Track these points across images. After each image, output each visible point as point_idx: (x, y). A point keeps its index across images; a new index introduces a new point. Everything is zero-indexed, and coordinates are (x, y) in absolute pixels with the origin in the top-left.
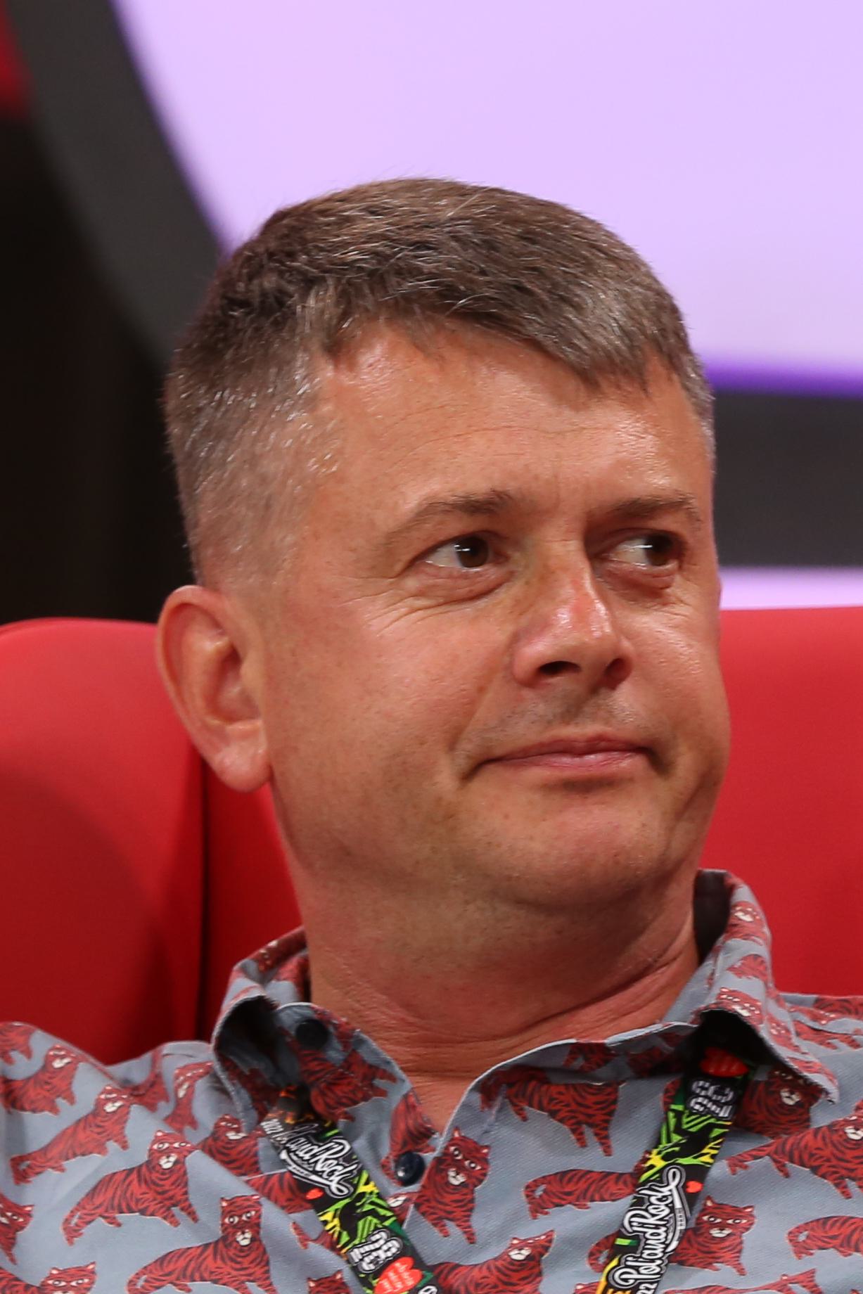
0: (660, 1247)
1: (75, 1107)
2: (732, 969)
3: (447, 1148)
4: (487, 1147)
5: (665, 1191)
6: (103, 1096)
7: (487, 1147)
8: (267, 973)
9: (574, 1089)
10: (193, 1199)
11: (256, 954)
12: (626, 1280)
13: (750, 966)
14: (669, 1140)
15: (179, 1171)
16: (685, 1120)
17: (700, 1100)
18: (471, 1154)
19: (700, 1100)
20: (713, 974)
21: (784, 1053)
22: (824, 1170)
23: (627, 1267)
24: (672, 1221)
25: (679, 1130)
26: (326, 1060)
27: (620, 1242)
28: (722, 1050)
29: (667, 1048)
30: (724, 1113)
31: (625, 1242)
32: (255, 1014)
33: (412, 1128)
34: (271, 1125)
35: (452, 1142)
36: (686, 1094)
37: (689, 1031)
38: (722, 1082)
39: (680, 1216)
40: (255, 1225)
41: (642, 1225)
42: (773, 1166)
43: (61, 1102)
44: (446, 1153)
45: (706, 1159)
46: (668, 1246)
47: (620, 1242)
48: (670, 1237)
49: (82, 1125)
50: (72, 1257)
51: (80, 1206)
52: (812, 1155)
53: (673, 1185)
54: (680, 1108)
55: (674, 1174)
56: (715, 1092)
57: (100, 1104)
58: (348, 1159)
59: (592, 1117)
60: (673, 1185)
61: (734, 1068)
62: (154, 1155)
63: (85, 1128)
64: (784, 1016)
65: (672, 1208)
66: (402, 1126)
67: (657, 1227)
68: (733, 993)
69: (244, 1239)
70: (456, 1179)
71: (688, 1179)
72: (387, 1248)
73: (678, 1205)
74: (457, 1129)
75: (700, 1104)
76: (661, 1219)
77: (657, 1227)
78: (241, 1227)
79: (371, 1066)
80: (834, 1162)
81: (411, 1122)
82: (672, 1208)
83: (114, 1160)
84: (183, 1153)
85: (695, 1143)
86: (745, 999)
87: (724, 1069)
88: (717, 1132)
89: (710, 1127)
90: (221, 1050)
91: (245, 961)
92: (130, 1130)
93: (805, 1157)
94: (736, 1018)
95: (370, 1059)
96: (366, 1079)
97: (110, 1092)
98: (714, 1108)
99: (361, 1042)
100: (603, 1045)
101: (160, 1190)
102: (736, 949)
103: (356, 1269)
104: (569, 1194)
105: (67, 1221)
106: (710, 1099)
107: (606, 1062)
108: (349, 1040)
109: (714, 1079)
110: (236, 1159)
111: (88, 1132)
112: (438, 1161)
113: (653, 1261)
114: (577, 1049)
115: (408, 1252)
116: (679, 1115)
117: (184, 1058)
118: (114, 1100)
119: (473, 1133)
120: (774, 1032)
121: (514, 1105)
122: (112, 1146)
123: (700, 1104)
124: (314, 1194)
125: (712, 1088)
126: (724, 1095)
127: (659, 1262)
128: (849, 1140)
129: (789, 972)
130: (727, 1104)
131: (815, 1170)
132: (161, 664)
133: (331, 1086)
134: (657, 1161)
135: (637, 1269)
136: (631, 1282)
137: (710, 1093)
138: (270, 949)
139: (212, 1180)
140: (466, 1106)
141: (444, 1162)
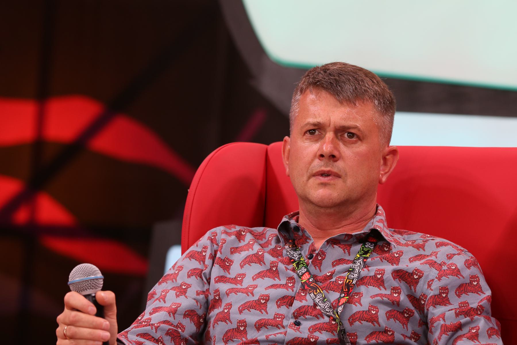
8: (291, 217)
9: (344, 241)
10: (265, 260)
13: (381, 221)
15: (262, 256)
18: (322, 253)
21: (386, 238)
25: (363, 250)
28: (375, 236)
29: (363, 236)
30: (372, 248)
32: (287, 223)
34: (287, 247)
35: (320, 251)
36: (365, 244)
38: (372, 243)
40: (277, 266)
43: (242, 241)
44: (319, 253)
50: (242, 271)
51: (243, 261)
57: (249, 242)
58: (300, 254)
62: (258, 252)
64: (388, 231)
65: (361, 264)
69: (274, 269)
70: (320, 258)
72: (304, 270)
78: (274, 267)
82: (361, 264)
83: (251, 252)
84: (264, 252)
85: (366, 253)
86: (379, 227)
89: (369, 250)
90: (279, 230)
94: (377, 230)
95: (307, 235)
96: (305, 239)
101: (258, 259)
102: (378, 218)
103: (298, 275)
105: (240, 264)
108: (303, 231)
110: (274, 253)
112: (317, 254)
114: (346, 235)
115: (308, 271)
116: (363, 248)
117: (271, 232)
119: (324, 250)
122: (250, 250)
124: (292, 260)
129: (391, 223)
132: (282, 151)
134: (358, 256)
139: (268, 258)
140: (324, 244)
141: (318, 255)
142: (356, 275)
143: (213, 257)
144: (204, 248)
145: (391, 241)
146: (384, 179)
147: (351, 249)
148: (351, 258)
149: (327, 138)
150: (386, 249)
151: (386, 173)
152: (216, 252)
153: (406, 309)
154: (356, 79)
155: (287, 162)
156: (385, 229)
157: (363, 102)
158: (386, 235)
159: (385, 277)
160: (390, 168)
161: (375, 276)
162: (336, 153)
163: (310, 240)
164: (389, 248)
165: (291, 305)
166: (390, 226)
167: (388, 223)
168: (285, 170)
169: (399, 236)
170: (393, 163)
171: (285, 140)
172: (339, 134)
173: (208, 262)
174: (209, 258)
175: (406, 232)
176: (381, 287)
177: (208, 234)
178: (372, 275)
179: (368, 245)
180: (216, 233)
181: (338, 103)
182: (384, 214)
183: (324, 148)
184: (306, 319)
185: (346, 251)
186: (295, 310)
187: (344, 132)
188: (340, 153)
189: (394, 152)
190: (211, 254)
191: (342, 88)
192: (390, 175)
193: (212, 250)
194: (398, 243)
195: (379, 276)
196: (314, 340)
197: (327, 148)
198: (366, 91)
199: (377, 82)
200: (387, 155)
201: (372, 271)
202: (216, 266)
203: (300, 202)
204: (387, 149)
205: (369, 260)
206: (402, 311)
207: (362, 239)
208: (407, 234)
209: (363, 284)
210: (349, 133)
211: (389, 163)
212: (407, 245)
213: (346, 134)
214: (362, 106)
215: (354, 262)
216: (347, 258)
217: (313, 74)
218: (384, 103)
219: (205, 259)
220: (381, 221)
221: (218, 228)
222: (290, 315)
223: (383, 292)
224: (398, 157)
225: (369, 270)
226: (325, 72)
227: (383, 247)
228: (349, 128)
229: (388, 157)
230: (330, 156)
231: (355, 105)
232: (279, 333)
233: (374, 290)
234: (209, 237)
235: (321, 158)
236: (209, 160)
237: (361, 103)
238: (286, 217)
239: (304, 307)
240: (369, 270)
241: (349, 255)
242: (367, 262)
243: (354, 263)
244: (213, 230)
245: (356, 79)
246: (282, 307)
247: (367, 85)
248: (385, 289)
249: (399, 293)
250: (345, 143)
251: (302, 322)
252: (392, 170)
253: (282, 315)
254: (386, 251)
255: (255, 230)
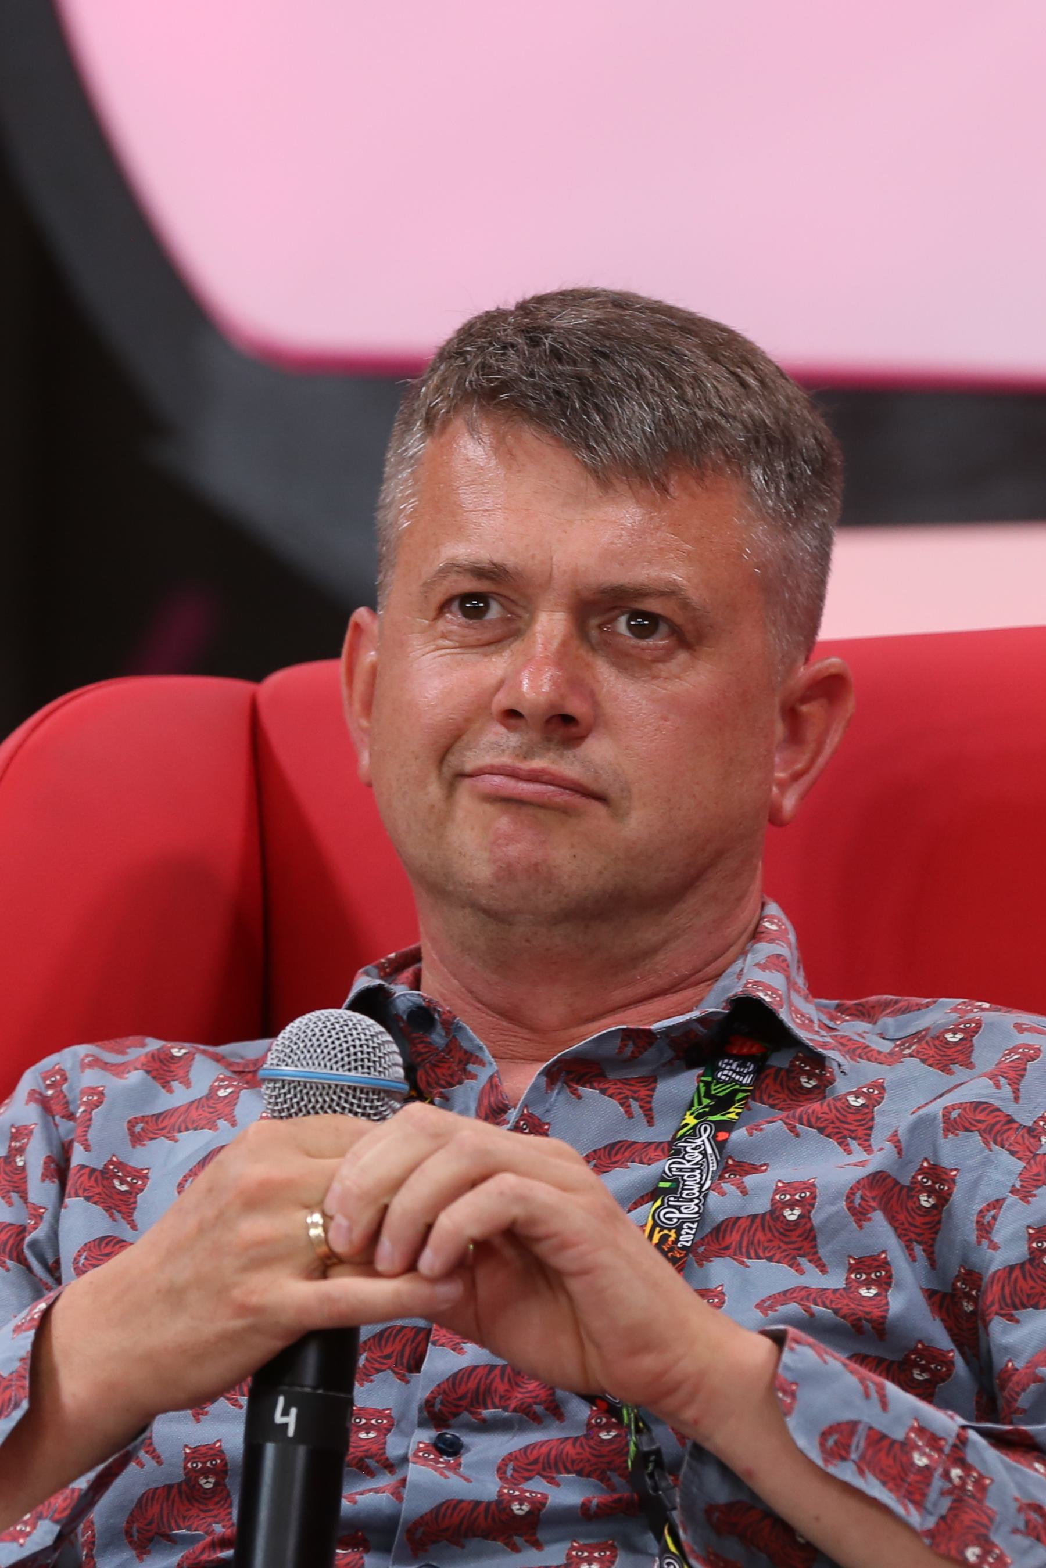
0: (697, 1187)
1: (190, 1090)
2: (757, 965)
3: (518, 1122)
4: (548, 1124)
5: (699, 1142)
6: (216, 1084)
7: (548, 1124)
11: (377, 962)
12: (670, 1219)
13: (776, 963)
14: (700, 1103)
16: (713, 1087)
17: (726, 1072)
19: (726, 1072)
20: (742, 970)
21: (803, 1035)
22: (829, 1130)
23: (669, 1206)
24: (705, 1164)
25: (708, 1095)
26: (430, 1043)
27: (662, 1185)
28: (751, 1027)
29: (701, 1030)
30: (747, 1080)
31: (667, 1185)
33: (493, 1104)
36: (714, 1069)
37: (721, 1016)
38: (743, 1060)
39: (712, 1160)
41: (680, 1170)
42: (785, 1128)
45: (733, 1116)
46: (702, 1185)
47: (662, 1185)
48: (704, 1178)
49: (195, 1105)
52: (818, 1118)
53: (704, 1137)
54: (709, 1079)
55: (705, 1129)
56: (738, 1066)
57: (213, 1090)
59: (638, 1094)
60: (704, 1137)
61: (754, 1050)
63: (197, 1108)
64: (809, 1009)
65: (705, 1155)
66: (486, 1102)
67: (693, 1170)
68: (757, 983)
71: (717, 1131)
73: (709, 1151)
74: (526, 1106)
75: (727, 1075)
76: (696, 1164)
77: (693, 1170)
79: (466, 1052)
80: (838, 1124)
81: (492, 1099)
82: (705, 1155)
85: (723, 1104)
86: (767, 988)
87: (745, 1050)
88: (741, 1095)
89: (735, 1092)
91: (368, 967)
92: (239, 1111)
93: (813, 1120)
94: (759, 1002)
95: (465, 1045)
97: (223, 1080)
98: (737, 1077)
99: (460, 1028)
100: (650, 1031)
102: (764, 950)
104: (616, 1162)
106: (734, 1071)
107: (650, 1045)
108: (451, 1027)
109: (736, 1058)
111: (200, 1112)
113: (691, 1200)
114: (628, 1034)
116: (708, 1085)
118: (226, 1087)
119: (538, 1111)
120: (798, 1021)
121: (569, 1087)
122: (222, 1123)
123: (727, 1075)
125: (736, 1064)
126: (745, 1067)
127: (697, 1201)
128: (850, 1106)
130: (749, 1073)
131: (821, 1131)
133: (434, 1066)
134: (691, 1120)
135: (678, 1208)
136: (675, 1220)
137: (734, 1067)
138: (389, 960)
142: (690, 1209)
143: (59, 1169)
144: (14, 1137)
145: (825, 1045)
146: (789, 803)
147: (657, 1094)
148: (661, 1132)
149: (540, 639)
150: (807, 1083)
151: (796, 777)
152: (65, 1150)
153: (915, 1351)
154: (670, 377)
155: (364, 723)
156: (798, 1001)
157: (700, 479)
158: (802, 1026)
159: (817, 1217)
160: (817, 753)
161: (776, 1211)
162: (576, 706)
163: (482, 1063)
164: (820, 1077)
165: (416, 1366)
166: (817, 989)
167: (809, 977)
168: (353, 759)
169: (862, 1026)
170: (831, 734)
171: (357, 626)
172: (594, 622)
173: (40, 1190)
174: (44, 1177)
175: (887, 1004)
176: (803, 1262)
177: (29, 1080)
178: (760, 1211)
179: (728, 1071)
180: (61, 1072)
181: (592, 483)
182: (792, 937)
183: (525, 686)
184: (486, 1427)
185: (635, 1105)
186: (433, 1387)
187: (617, 616)
188: (595, 704)
189: (830, 687)
190: (49, 1160)
191: (606, 419)
192: (814, 783)
193: (49, 1141)
194: (859, 1051)
195: (792, 1215)
196: (526, 1507)
197: (535, 688)
198: (710, 426)
199: (762, 382)
200: (804, 699)
201: (758, 1192)
202: (75, 1204)
203: (423, 902)
204: (804, 673)
205: (739, 1135)
206: (898, 1357)
207: (696, 1048)
208: (894, 1014)
209: (722, 1252)
210: (635, 614)
211: (811, 734)
212: (892, 1059)
213: (623, 620)
214: (693, 496)
215: (672, 1149)
216: (642, 1134)
217: (481, 349)
218: (790, 477)
219: (24, 1180)
220: (776, 963)
221: (68, 1052)
222: (414, 1414)
223: (813, 1279)
224: (850, 705)
225: (744, 1192)
226: (535, 342)
227: (793, 1073)
228: (641, 593)
229: (804, 708)
230: (549, 721)
231: (664, 490)
232: (370, 1490)
233: (772, 1276)
234: (32, 1093)
235: (512, 722)
236: (8, 765)
237: (692, 483)
238: (367, 974)
239: (471, 1371)
240: (744, 1192)
241: (650, 1122)
242: (729, 1146)
243: (678, 1152)
244: (49, 1062)
245: (670, 377)
246: (376, 1377)
247: (716, 402)
248: (823, 1268)
249: (885, 1283)
250: (625, 662)
251: (466, 1439)
252: (821, 761)
253: (379, 1414)
254: (809, 1091)
255: (234, 1054)
